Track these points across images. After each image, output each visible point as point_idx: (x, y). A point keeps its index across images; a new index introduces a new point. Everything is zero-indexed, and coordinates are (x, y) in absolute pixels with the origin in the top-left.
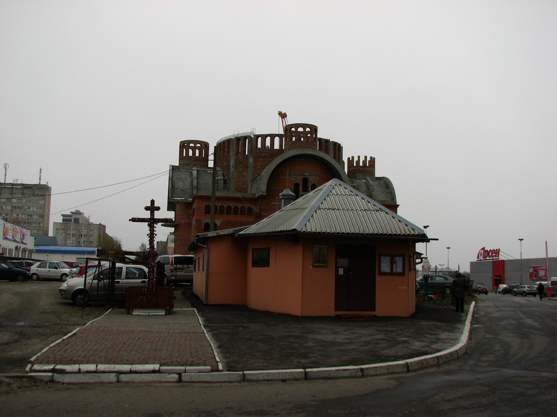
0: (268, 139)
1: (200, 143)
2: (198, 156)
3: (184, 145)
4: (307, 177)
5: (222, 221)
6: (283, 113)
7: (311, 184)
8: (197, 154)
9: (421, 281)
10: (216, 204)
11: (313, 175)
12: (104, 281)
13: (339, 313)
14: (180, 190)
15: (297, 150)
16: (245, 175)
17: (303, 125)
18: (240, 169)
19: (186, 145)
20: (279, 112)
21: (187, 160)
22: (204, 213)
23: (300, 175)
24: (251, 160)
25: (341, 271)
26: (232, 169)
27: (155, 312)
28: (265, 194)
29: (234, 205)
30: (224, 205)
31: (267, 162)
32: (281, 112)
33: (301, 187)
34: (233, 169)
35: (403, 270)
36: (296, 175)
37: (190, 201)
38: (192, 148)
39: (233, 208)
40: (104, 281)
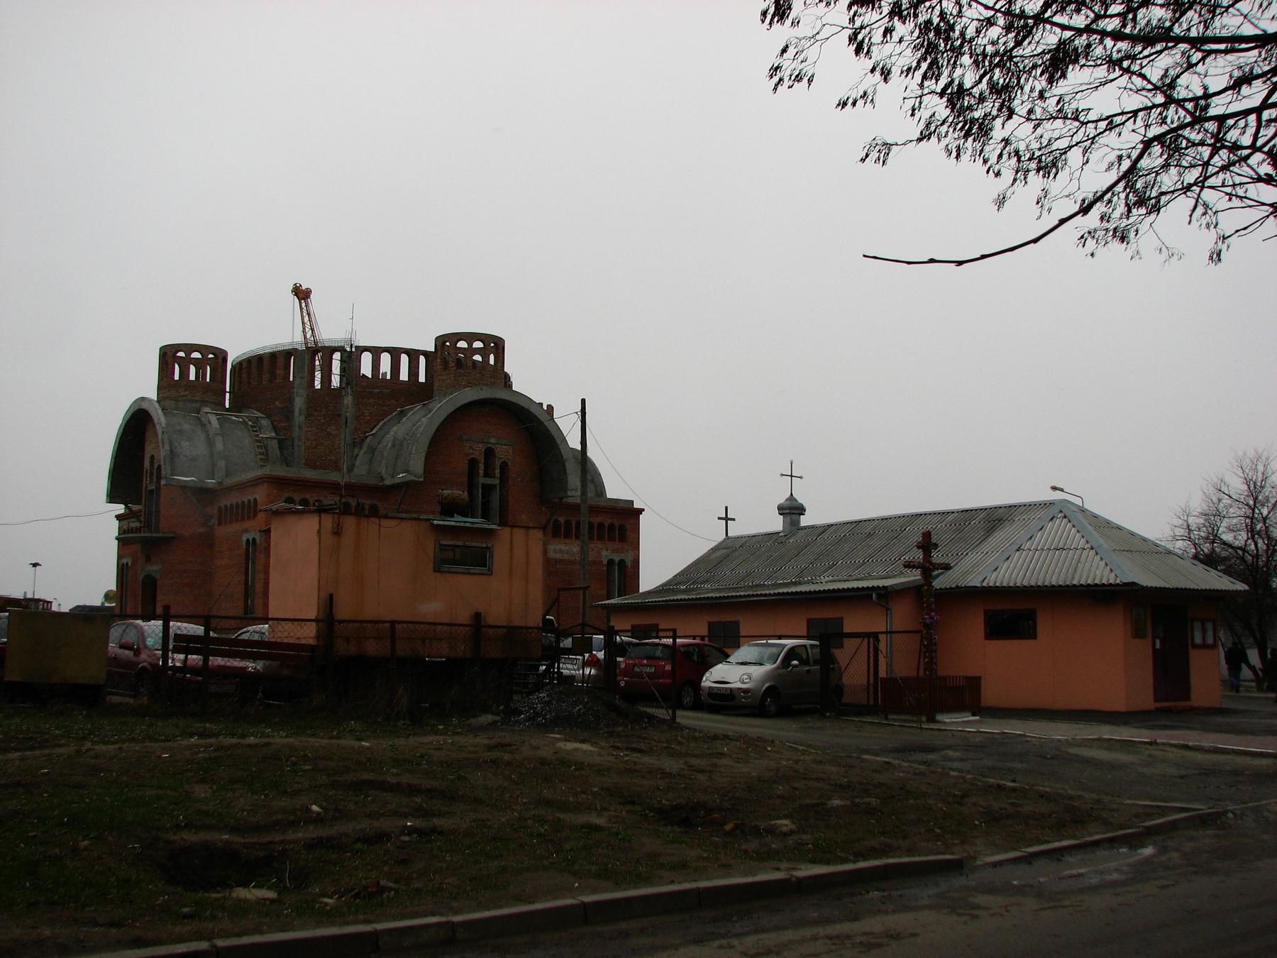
0: (386, 359)
1: (215, 352)
2: (194, 379)
3: (168, 356)
7: (500, 462)
8: (192, 377)
10: (591, 520)
13: (1159, 705)
14: (185, 459)
15: (482, 389)
16: (334, 432)
17: (484, 338)
18: (320, 418)
19: (448, 344)
20: (295, 284)
21: (186, 390)
23: (480, 442)
24: (348, 400)
25: (1158, 645)
26: (298, 418)
27: (958, 716)
28: (422, 479)
31: (386, 409)
33: (482, 466)
34: (302, 418)
35: (846, 633)
36: (473, 441)
37: (211, 486)
38: (196, 362)
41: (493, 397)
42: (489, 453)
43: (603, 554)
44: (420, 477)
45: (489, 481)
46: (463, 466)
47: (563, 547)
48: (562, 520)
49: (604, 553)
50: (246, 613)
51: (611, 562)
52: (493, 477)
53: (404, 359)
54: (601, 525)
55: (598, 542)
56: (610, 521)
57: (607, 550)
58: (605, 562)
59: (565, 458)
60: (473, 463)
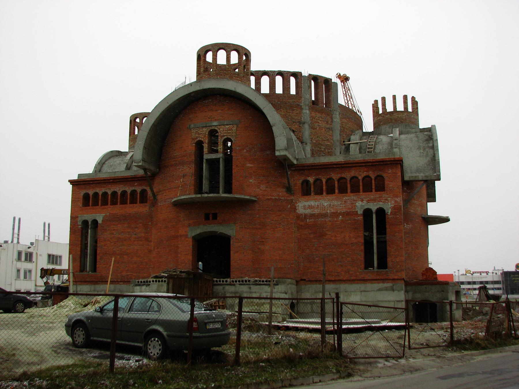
4: (216, 128)
5: (105, 216)
6: (342, 75)
9: (99, 314)
11: (225, 123)
12: (327, 299)
22: (81, 205)
29: (122, 190)
30: (107, 191)
32: (340, 74)
39: (119, 194)
40: (327, 299)
41: (201, 88)
42: (213, 134)
43: (357, 204)
44: (140, 162)
45: (213, 156)
46: (191, 148)
47: (312, 203)
48: (311, 180)
49: (359, 204)
50: (271, 302)
51: (367, 213)
52: (216, 151)
53: (279, 80)
54: (354, 179)
55: (351, 194)
56: (365, 174)
57: (362, 201)
58: (360, 212)
59: (271, 123)
60: (199, 145)
